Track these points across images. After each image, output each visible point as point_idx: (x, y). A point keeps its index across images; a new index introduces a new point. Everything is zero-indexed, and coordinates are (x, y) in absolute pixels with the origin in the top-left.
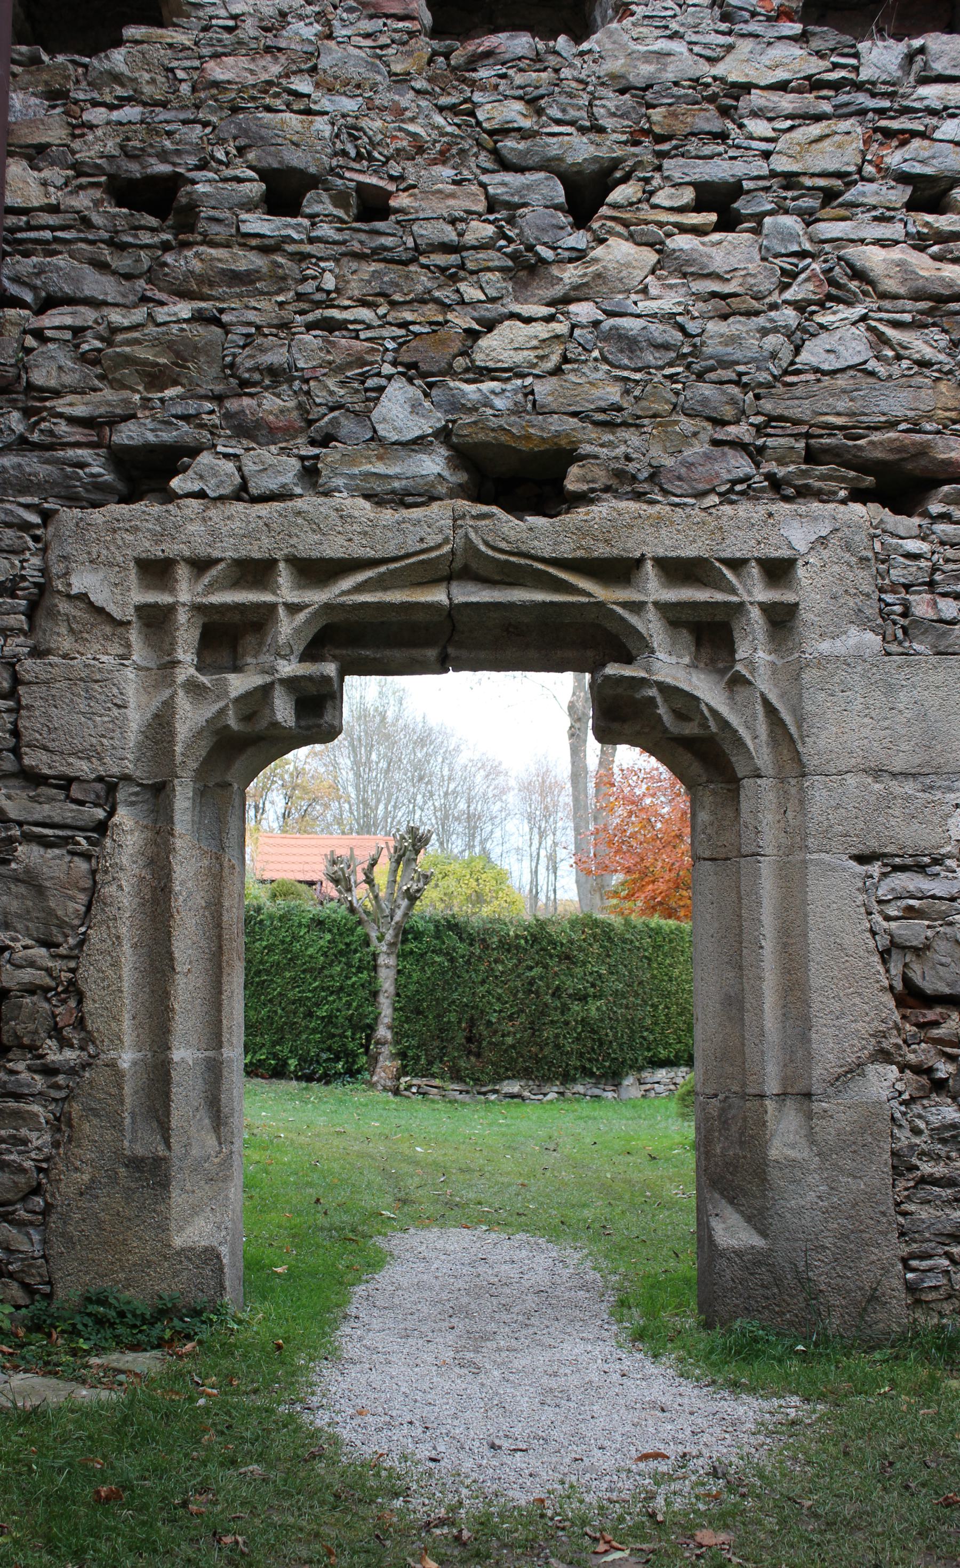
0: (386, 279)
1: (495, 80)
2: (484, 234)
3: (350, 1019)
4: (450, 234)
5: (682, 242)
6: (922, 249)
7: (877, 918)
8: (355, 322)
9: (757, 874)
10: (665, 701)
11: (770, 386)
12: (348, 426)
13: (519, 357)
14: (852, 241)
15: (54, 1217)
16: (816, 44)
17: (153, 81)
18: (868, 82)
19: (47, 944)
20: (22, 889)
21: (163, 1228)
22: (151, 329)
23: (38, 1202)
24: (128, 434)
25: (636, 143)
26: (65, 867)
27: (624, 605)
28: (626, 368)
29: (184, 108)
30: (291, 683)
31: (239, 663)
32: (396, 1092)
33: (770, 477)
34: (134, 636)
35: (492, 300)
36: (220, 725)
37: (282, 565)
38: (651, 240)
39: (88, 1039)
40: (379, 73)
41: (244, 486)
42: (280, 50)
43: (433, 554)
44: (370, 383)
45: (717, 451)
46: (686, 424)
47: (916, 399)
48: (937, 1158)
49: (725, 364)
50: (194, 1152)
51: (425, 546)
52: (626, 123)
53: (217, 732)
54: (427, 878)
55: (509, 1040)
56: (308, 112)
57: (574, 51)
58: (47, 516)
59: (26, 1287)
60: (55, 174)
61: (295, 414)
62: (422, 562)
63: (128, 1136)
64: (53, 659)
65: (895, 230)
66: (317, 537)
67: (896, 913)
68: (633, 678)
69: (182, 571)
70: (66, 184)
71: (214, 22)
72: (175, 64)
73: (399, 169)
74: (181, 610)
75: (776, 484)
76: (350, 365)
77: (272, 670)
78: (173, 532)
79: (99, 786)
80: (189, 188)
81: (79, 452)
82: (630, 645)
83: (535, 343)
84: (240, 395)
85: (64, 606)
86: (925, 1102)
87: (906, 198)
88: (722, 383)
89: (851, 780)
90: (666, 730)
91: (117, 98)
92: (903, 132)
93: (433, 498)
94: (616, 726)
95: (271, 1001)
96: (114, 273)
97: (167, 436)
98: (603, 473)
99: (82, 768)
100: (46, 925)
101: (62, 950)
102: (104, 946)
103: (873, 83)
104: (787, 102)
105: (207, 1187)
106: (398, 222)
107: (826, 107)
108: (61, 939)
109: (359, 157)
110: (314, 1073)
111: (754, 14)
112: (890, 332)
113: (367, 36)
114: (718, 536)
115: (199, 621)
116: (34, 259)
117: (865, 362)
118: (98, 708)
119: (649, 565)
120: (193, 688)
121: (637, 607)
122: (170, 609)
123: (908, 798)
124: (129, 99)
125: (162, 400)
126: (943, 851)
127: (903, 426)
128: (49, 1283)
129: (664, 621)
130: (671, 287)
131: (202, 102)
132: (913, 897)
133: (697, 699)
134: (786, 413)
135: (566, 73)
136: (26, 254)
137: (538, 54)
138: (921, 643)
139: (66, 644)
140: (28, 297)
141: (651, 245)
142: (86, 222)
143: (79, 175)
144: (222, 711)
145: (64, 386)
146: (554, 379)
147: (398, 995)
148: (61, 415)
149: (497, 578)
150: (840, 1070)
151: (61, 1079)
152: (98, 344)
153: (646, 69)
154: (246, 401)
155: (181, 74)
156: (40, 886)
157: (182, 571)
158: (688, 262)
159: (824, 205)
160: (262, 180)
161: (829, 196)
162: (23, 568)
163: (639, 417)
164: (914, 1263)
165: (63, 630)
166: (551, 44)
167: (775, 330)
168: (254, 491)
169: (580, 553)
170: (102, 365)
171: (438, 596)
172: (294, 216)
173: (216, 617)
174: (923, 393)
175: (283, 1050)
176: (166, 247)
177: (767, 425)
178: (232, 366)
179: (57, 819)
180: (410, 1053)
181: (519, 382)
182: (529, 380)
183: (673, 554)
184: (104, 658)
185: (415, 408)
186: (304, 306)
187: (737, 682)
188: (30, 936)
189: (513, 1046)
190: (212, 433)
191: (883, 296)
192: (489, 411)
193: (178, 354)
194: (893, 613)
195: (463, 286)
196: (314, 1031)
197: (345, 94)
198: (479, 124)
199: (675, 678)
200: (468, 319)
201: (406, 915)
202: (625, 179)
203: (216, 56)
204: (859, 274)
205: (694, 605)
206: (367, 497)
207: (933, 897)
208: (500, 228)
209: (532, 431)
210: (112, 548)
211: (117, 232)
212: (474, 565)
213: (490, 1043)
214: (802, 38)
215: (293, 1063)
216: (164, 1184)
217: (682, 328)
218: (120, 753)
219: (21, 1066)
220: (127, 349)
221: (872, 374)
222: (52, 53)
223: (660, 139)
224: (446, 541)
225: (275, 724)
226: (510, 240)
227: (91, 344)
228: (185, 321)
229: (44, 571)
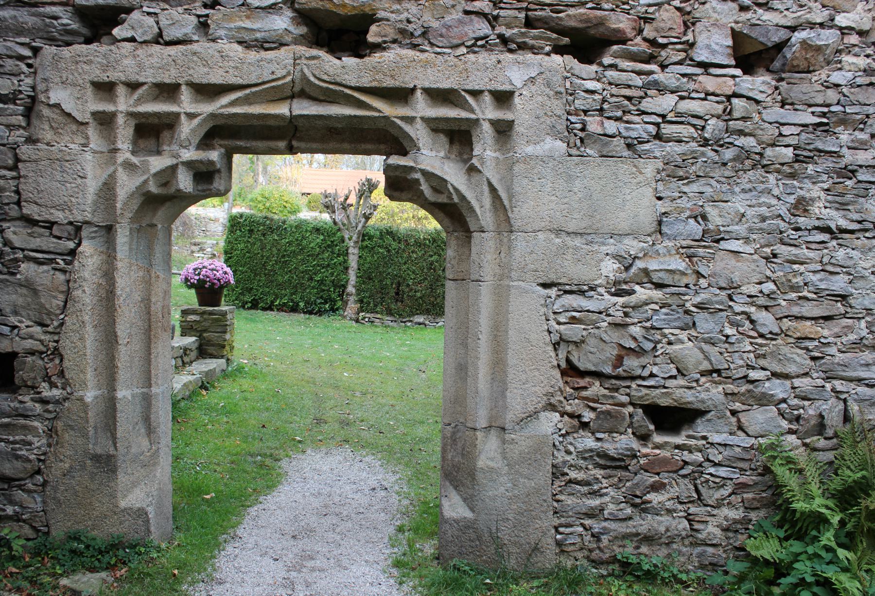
3: (333, 282)
9: (478, 294)
10: (427, 181)
15: (48, 488)
20: (24, 291)
23: (39, 479)
27: (402, 118)
30: (189, 164)
31: (161, 149)
32: (357, 321)
33: (501, 37)
34: (92, 132)
36: (144, 191)
37: (183, 88)
41: (160, 34)
43: (280, 83)
45: (467, 18)
51: (275, 77)
53: (144, 194)
54: (375, 207)
55: (419, 294)
58: (36, 51)
62: (273, 87)
64: (40, 146)
66: (206, 70)
68: (405, 166)
69: (121, 90)
75: (504, 40)
78: (114, 64)
79: (70, 228)
81: (54, 9)
82: (405, 144)
85: (46, 112)
86: (575, 435)
90: (426, 199)
93: (283, 45)
94: (396, 194)
95: (290, 271)
99: (59, 216)
101: (50, 329)
102: (75, 327)
108: (49, 322)
110: (313, 310)
114: (464, 75)
115: (133, 123)
119: (419, 93)
120: (129, 166)
121: (410, 120)
122: (113, 115)
123: (576, 248)
126: (596, 283)
128: (47, 526)
129: (428, 129)
133: (446, 181)
138: (591, 149)
139: (49, 136)
144: (145, 182)
147: (359, 269)
149: (322, 98)
151: (50, 407)
156: (35, 289)
162: (20, 85)
164: (561, 529)
165: (47, 127)
168: (167, 38)
169: (375, 84)
173: (143, 120)
175: (296, 298)
179: (45, 248)
180: (365, 300)
183: (435, 86)
184: (72, 146)
187: (472, 170)
189: (421, 298)
196: (313, 288)
199: (433, 167)
201: (363, 227)
205: (447, 120)
206: (240, 43)
207: (588, 311)
210: (76, 74)
212: (307, 90)
213: (408, 296)
215: (302, 304)
216: (114, 471)
218: (82, 207)
224: (289, 74)
225: (179, 191)
229: (34, 88)
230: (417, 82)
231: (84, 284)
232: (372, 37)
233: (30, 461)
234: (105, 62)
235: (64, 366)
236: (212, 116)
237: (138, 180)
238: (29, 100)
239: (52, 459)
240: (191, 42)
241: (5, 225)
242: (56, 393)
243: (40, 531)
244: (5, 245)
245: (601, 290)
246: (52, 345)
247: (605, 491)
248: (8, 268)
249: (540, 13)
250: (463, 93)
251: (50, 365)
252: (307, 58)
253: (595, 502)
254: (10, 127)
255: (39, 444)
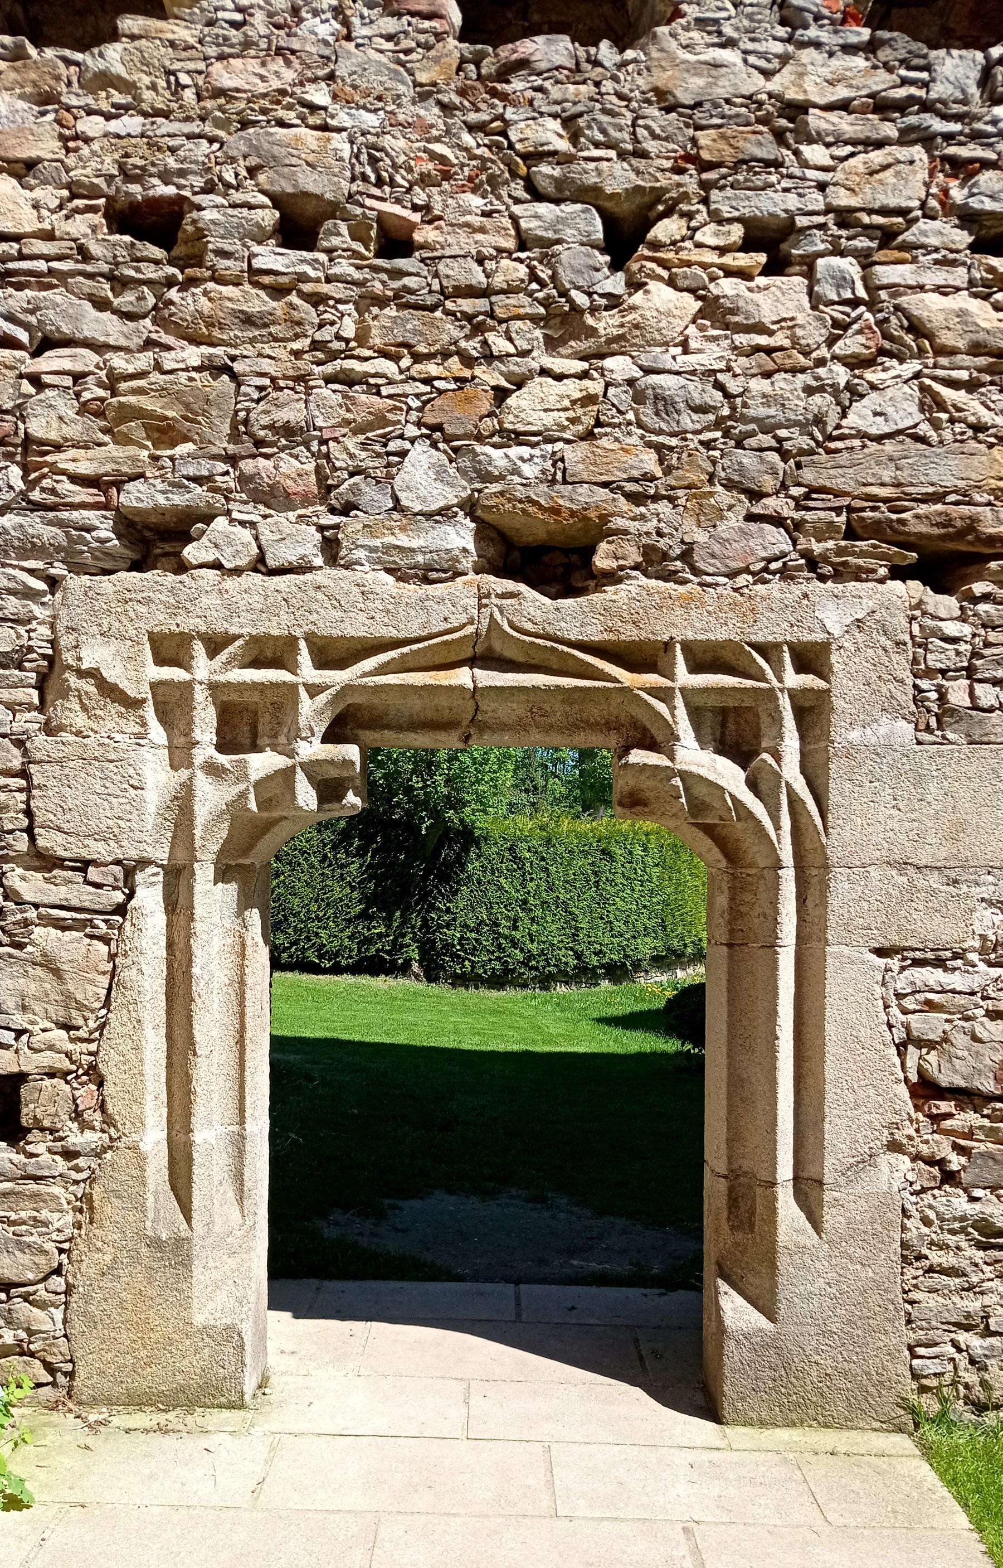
0: (409, 326)
1: (529, 94)
2: (515, 276)
4: (478, 277)
5: (727, 287)
6: (986, 297)
7: (895, 1010)
8: (376, 375)
11: (811, 452)
12: (371, 494)
13: (549, 419)
14: (910, 287)
15: (75, 1297)
16: (884, 54)
17: (153, 87)
18: (939, 100)
19: (67, 1027)
20: (39, 971)
21: (185, 1304)
22: (156, 377)
23: (58, 1283)
24: (136, 496)
25: (680, 171)
26: (84, 950)
27: (652, 691)
28: (660, 432)
29: (188, 119)
30: (311, 768)
34: (149, 712)
35: (524, 354)
38: (694, 285)
39: (109, 1121)
40: (403, 83)
41: (261, 559)
42: (293, 52)
44: (392, 446)
45: (753, 526)
46: (723, 496)
47: (967, 466)
48: (943, 1247)
49: (768, 428)
50: (217, 1229)
51: (449, 626)
52: (672, 146)
56: (325, 128)
57: (618, 58)
59: (50, 1368)
60: (50, 195)
61: (313, 478)
63: (151, 1215)
64: (66, 736)
65: (959, 276)
67: (913, 1007)
70: (61, 207)
71: (220, 14)
72: (177, 66)
73: (424, 196)
74: (198, 688)
75: (812, 563)
76: (369, 427)
77: (291, 754)
78: (188, 605)
79: (117, 869)
80: (195, 214)
81: (85, 513)
83: (566, 403)
84: (253, 456)
85: (73, 681)
86: (936, 1192)
87: (970, 239)
88: (761, 450)
89: (874, 872)
91: (114, 105)
92: (972, 161)
96: (115, 312)
97: (178, 499)
98: (634, 549)
99: (97, 849)
100: (66, 1007)
101: (82, 1034)
102: (124, 1030)
103: (944, 103)
104: (845, 124)
105: (230, 1261)
106: (423, 260)
107: (890, 130)
108: (80, 1022)
109: (380, 183)
111: (818, 17)
112: (947, 393)
113: (389, 38)
114: (750, 619)
116: (28, 293)
117: (915, 426)
118: (112, 789)
120: (213, 770)
121: (664, 695)
122: (187, 687)
123: (933, 892)
124: (127, 108)
125: (172, 459)
126: (965, 946)
127: (952, 498)
128: (71, 1361)
130: (715, 339)
131: (209, 113)
132: (932, 991)
134: (828, 484)
135: (608, 86)
136: (19, 287)
137: (577, 64)
138: (954, 731)
139: (80, 720)
140: (23, 336)
141: (692, 291)
142: (84, 254)
143: (73, 196)
144: (243, 795)
145: (66, 440)
146: (584, 444)
148: (63, 472)
150: (852, 1160)
151: (81, 1162)
152: (101, 393)
153: (696, 83)
154: (261, 462)
155: (184, 79)
156: (58, 969)
157: (199, 648)
158: (733, 312)
159: (880, 248)
160: (275, 206)
161: (887, 237)
163: (673, 488)
164: (921, 1351)
166: (593, 50)
167: (821, 389)
168: (271, 563)
170: (111, 418)
171: (462, 677)
172: (310, 249)
174: (975, 461)
176: (170, 282)
177: (807, 497)
178: (246, 422)
179: (75, 902)
181: (549, 447)
182: (560, 445)
183: (703, 637)
185: (440, 474)
186: (320, 355)
188: (49, 1018)
190: (226, 498)
191: (941, 351)
192: (517, 479)
193: (187, 406)
194: (928, 699)
195: (491, 337)
197: (364, 108)
198: (511, 146)
200: (496, 374)
202: (667, 214)
203: (221, 57)
204: (916, 328)
206: (389, 571)
207: (954, 992)
208: (532, 269)
209: (561, 502)
210: (126, 622)
211: (117, 264)
212: (497, 646)
214: (871, 48)
216: (187, 1264)
217: (719, 386)
218: (137, 836)
219: (40, 1148)
220: (132, 399)
221: (923, 440)
222: (38, 44)
223: (710, 166)
226: (543, 285)
227: (93, 391)
228: (195, 369)
229: (53, 643)
230: (674, 632)
231: (141, 959)
232: (602, 560)
233: (45, 1252)
234: (173, 602)
235: (105, 1093)
236: (347, 689)
237: (229, 792)
238: (46, 663)
239: (82, 1247)
240: (310, 569)
241: (6, 867)
242: (91, 1138)
243: (59, 1370)
244: (6, 898)
245: (973, 957)
246: (86, 1059)
247: (990, 1284)
248: (10, 936)
249: (871, 514)
250: (748, 648)
251: (82, 1091)
252: (497, 596)
253: (973, 1304)
254: (12, 707)
255: (61, 1222)
